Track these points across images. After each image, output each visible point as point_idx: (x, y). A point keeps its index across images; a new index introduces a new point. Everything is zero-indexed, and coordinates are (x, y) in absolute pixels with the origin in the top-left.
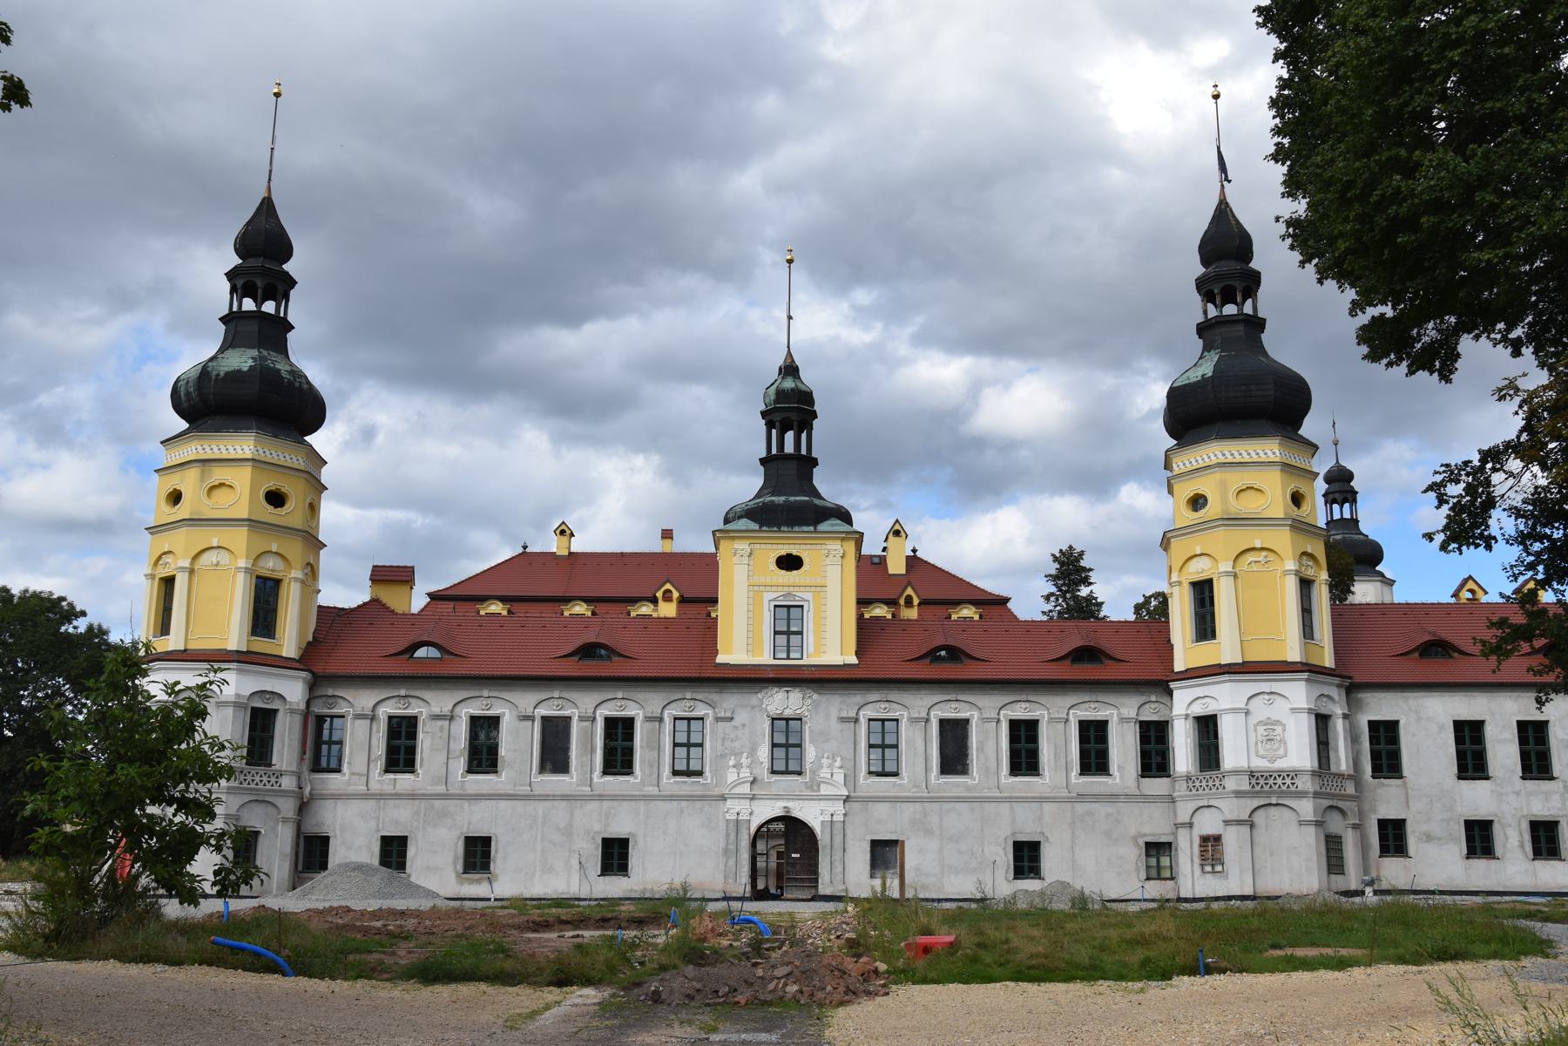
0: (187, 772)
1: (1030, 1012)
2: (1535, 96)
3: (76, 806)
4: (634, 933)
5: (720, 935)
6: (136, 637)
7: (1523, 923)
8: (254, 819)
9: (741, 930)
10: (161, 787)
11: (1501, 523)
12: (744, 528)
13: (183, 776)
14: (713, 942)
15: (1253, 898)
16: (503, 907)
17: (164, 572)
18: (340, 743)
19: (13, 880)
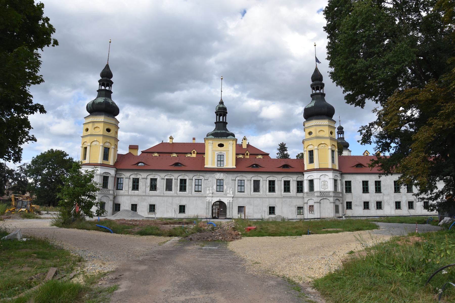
0: (90, 189)
1: (272, 243)
2: (380, 49)
3: (67, 196)
4: (186, 226)
5: (205, 226)
6: (79, 160)
7: (374, 222)
8: (104, 200)
9: (210, 225)
10: (84, 192)
11: (373, 139)
13: (89, 190)
14: (203, 228)
15: (320, 218)
16: (158, 220)
17: (85, 146)
18: (122, 184)
19: (55, 211)
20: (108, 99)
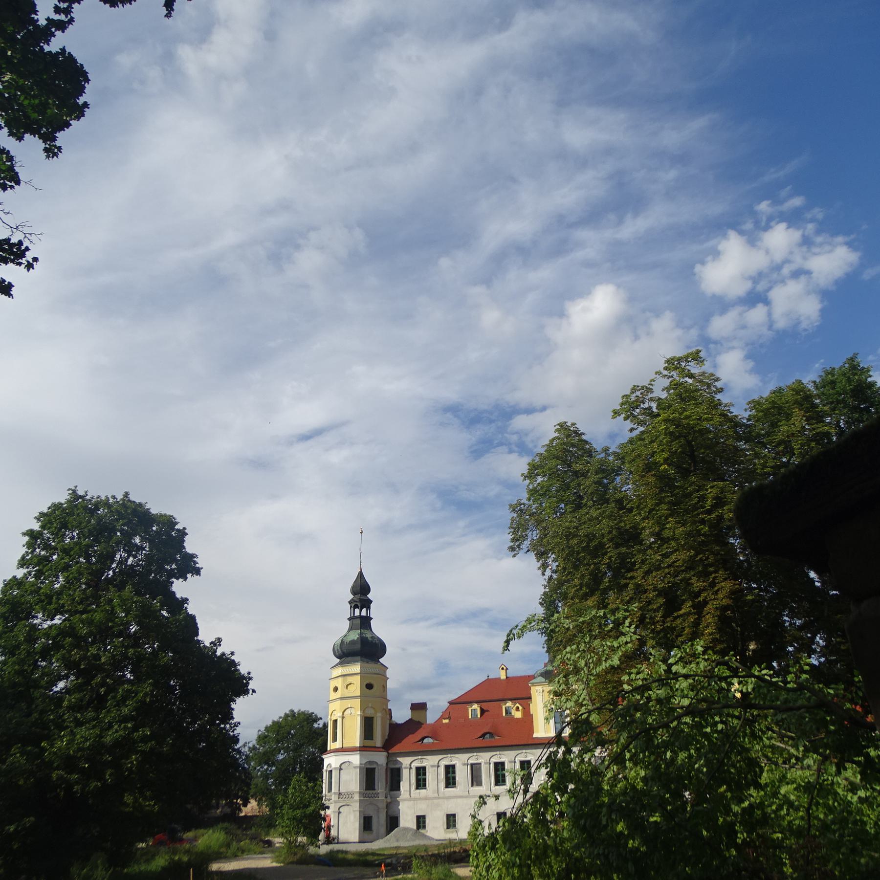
12: (538, 681)
20: (366, 632)
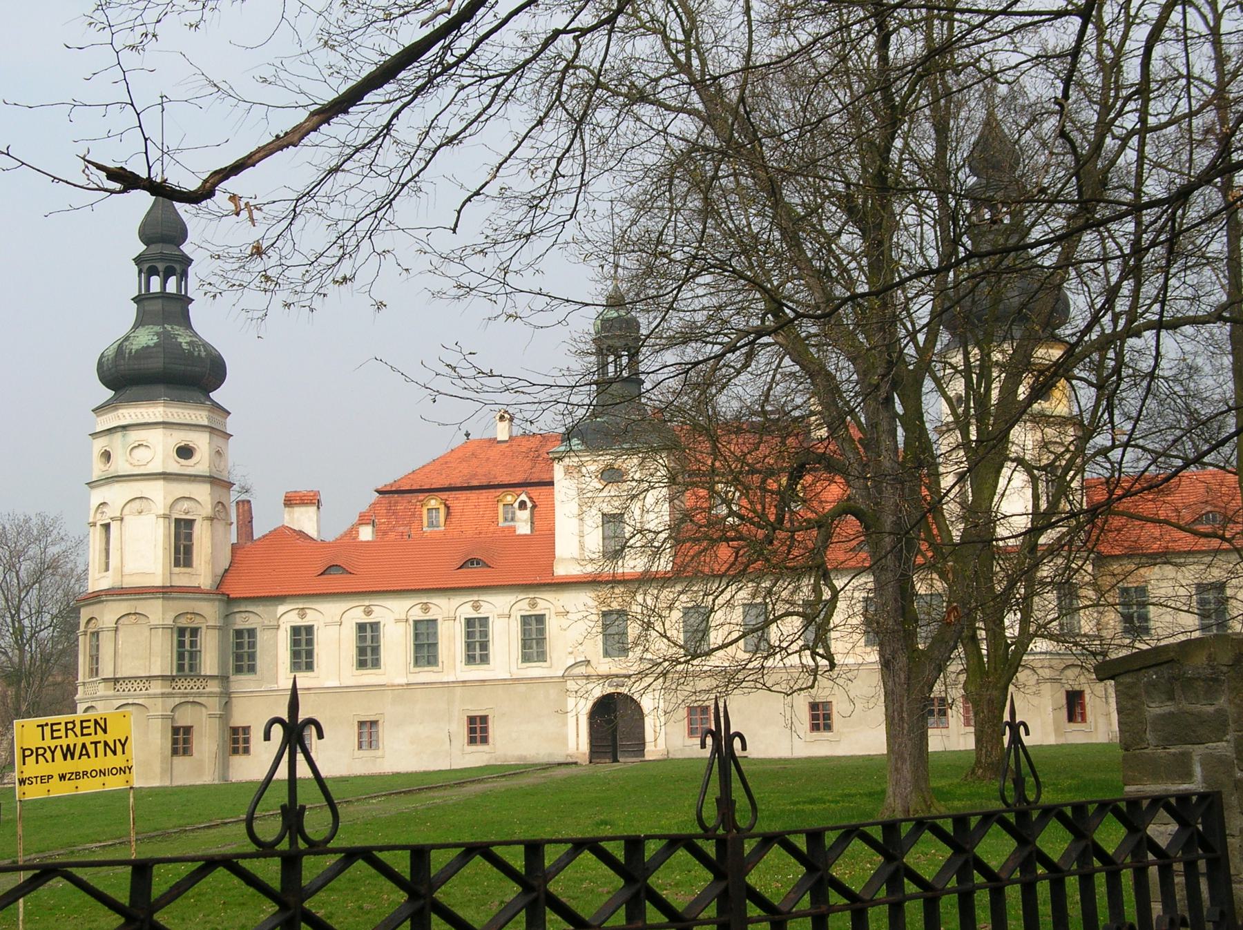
20: (178, 330)
